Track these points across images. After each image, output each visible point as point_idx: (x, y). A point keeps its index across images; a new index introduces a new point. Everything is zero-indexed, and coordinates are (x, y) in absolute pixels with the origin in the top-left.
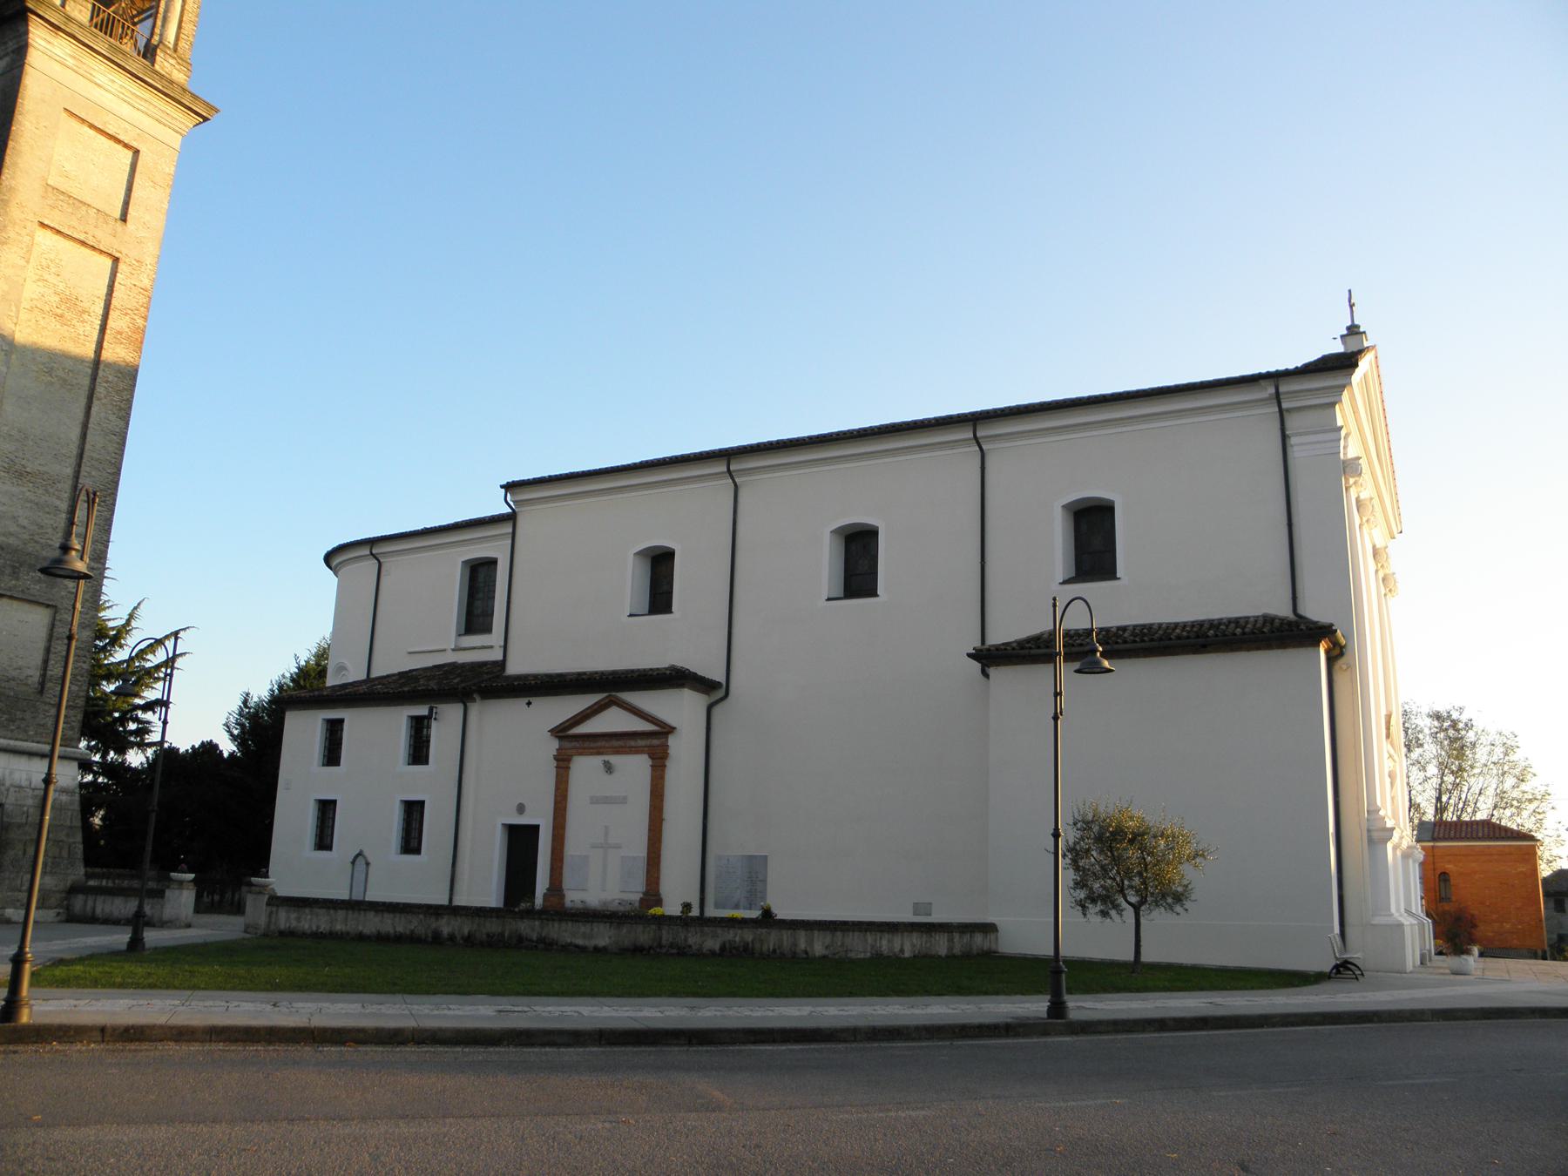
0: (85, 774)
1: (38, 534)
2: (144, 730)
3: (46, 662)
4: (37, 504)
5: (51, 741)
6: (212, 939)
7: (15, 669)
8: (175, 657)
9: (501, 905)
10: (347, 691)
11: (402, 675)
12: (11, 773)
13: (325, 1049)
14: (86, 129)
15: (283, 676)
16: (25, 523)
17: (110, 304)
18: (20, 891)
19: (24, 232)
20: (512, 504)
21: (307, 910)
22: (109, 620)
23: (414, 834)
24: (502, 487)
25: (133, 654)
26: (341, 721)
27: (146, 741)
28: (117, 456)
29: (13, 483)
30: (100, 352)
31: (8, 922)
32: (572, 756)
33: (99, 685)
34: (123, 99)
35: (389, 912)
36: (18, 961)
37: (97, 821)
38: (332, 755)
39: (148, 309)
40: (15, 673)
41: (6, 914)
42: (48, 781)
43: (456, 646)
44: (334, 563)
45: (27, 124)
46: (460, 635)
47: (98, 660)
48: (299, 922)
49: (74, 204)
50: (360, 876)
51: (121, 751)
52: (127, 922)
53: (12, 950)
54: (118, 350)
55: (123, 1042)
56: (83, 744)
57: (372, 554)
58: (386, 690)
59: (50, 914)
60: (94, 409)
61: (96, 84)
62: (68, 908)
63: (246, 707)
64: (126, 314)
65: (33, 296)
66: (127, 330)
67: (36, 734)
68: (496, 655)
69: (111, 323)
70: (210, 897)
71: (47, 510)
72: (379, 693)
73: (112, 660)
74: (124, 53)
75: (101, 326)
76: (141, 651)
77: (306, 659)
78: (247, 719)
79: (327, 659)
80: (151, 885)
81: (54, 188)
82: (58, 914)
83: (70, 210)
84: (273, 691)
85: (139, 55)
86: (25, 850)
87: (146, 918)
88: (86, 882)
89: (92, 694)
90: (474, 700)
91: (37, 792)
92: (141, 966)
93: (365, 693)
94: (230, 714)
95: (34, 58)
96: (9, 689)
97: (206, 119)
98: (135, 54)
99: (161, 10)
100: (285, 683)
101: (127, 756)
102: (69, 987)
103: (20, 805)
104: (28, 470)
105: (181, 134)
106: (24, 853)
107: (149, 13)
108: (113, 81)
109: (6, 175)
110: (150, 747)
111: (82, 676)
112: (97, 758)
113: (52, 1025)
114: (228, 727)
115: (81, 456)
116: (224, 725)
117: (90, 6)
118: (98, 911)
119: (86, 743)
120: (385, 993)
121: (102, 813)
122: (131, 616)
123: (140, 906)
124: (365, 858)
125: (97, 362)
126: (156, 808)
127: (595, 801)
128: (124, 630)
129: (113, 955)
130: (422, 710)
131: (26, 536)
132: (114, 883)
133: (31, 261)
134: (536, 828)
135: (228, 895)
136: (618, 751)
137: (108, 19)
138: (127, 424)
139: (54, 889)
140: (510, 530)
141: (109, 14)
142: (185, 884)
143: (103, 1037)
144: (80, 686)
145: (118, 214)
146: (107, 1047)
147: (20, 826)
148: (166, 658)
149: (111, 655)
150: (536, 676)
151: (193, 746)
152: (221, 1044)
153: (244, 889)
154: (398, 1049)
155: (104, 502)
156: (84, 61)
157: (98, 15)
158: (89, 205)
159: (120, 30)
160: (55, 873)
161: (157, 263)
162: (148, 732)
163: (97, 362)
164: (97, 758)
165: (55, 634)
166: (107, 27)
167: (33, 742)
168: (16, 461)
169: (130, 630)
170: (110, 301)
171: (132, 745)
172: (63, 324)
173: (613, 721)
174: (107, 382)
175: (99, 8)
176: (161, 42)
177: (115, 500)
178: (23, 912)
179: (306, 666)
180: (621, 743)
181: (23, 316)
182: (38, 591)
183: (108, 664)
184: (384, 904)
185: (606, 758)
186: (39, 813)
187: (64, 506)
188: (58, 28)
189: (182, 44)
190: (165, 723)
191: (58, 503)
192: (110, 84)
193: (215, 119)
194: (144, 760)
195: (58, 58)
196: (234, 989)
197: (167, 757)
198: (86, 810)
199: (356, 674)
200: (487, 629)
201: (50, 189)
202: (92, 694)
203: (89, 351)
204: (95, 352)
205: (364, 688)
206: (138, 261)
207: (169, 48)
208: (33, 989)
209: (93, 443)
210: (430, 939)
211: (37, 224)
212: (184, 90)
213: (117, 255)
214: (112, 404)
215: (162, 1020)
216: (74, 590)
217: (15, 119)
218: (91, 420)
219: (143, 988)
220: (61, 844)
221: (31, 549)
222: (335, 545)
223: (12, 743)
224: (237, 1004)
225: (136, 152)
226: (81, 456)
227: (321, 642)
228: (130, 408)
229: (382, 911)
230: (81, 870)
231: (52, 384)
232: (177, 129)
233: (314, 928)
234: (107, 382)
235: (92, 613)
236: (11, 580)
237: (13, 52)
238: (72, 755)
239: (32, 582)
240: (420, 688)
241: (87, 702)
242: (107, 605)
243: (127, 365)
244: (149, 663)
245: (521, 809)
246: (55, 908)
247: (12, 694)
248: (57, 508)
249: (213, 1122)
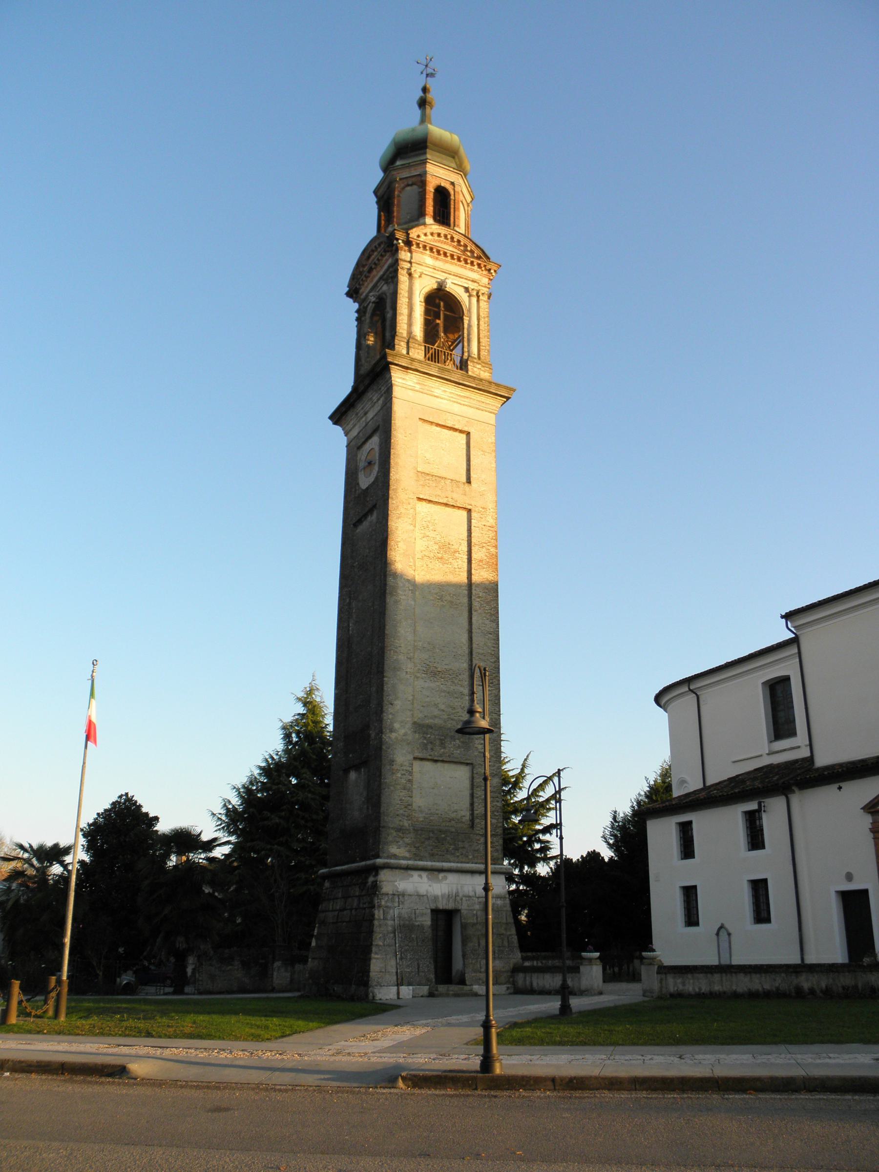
0: (510, 884)
1: (453, 714)
2: (545, 848)
3: (472, 804)
4: (448, 693)
5: (484, 862)
6: (620, 1003)
7: (453, 812)
8: (560, 790)
9: (846, 961)
10: (691, 798)
11: (731, 780)
12: (462, 887)
13: (730, 1096)
14: (434, 428)
15: (639, 794)
16: (442, 707)
17: (471, 542)
18: (481, 972)
19: (409, 507)
20: (793, 629)
21: (690, 976)
22: (509, 771)
23: (763, 907)
24: (782, 617)
25: (530, 793)
26: (690, 823)
27: (548, 856)
28: (495, 649)
29: (431, 681)
30: (471, 578)
31: (476, 995)
33: (510, 818)
34: (452, 401)
35: (756, 973)
36: (486, 1026)
37: (523, 918)
38: (687, 850)
39: (496, 540)
40: (453, 815)
41: (474, 990)
42: (486, 889)
43: (769, 751)
44: (663, 702)
45: (400, 435)
46: (771, 742)
47: (506, 801)
49: (436, 480)
50: (724, 945)
51: (532, 865)
52: (556, 992)
53: (481, 1017)
54: (482, 573)
55: (570, 1090)
56: (506, 862)
57: (690, 690)
58: (721, 794)
59: (503, 988)
60: (474, 619)
61: (435, 396)
62: (514, 983)
63: (616, 821)
64: (483, 547)
65: (422, 549)
66: (486, 558)
67: (474, 857)
68: (805, 753)
69: (474, 556)
70: (612, 970)
71: (456, 695)
72: (716, 797)
73: (516, 799)
74: (448, 371)
75: (468, 559)
76: (535, 790)
77: (654, 779)
78: (618, 831)
79: (670, 777)
80: (569, 963)
81: (422, 473)
82: (508, 988)
83: (434, 485)
84: (634, 807)
85: (457, 369)
86: (479, 942)
87: (569, 989)
88: (523, 963)
89: (506, 825)
90: (793, 792)
91: (481, 900)
92: (572, 1027)
93: (705, 798)
94: (605, 828)
95: (397, 392)
96: (452, 826)
97: (508, 398)
98: (455, 369)
99: (465, 335)
100: (641, 800)
101: (537, 869)
102: (524, 1045)
103: (471, 910)
104: (439, 670)
105: (494, 413)
106: (479, 945)
107: (458, 341)
108: (445, 391)
109: (393, 472)
110: (551, 860)
111: (498, 812)
112: (516, 872)
113: (517, 1076)
114: (605, 838)
115: (471, 653)
116: (602, 837)
117: (423, 348)
118: (535, 984)
119: (507, 862)
120: (769, 1044)
121: (526, 911)
122: (524, 766)
123: (564, 980)
124: (727, 930)
125: (470, 584)
126: (565, 905)
128: (520, 776)
129: (550, 1018)
130: (753, 806)
131: (446, 717)
132: (542, 963)
133: (417, 525)
135: (625, 967)
137: (435, 352)
138: (498, 624)
139: (503, 970)
140: (796, 651)
141: (435, 349)
142: (593, 961)
143: (554, 1086)
144: (497, 819)
145: (464, 479)
146: (559, 1095)
147: (474, 925)
148: (554, 792)
149: (514, 796)
150: (841, 765)
151: (582, 856)
152: (644, 1092)
153: (637, 962)
154: (793, 1097)
155: (492, 683)
156: (425, 384)
157: (429, 352)
158: (445, 478)
159: (443, 357)
160: (502, 958)
161: (496, 506)
162: (549, 849)
163: (470, 584)
164: (516, 872)
165: (475, 784)
166: (435, 358)
167: (472, 863)
168: (431, 664)
169: (524, 776)
170: (471, 540)
171: (539, 860)
172: (444, 564)
174: (479, 597)
175: (429, 347)
176: (469, 356)
177: (499, 681)
178: (484, 988)
179: (655, 785)
181: (419, 563)
182: (459, 754)
183: (513, 803)
184: (750, 966)
186: (484, 914)
187: (466, 691)
188: (407, 368)
189: (482, 353)
190: (561, 838)
191: (462, 689)
192: (443, 393)
193: (514, 397)
194: (549, 870)
195: (410, 387)
196: (645, 1044)
197: (565, 864)
198: (516, 913)
199: (694, 784)
200: (792, 733)
201: (420, 474)
202: (506, 825)
203: (463, 578)
204: (468, 578)
205: (703, 795)
206: (483, 508)
207: (475, 358)
208: (500, 1047)
209: (477, 643)
210: (794, 994)
211: (416, 499)
212: (490, 382)
213: (469, 507)
214: (485, 612)
215: (595, 1072)
216: (483, 750)
217: (392, 435)
218: (474, 626)
219: (577, 1045)
220: (502, 936)
221: (449, 725)
222: (661, 688)
223: (459, 865)
224: (650, 1057)
225: (468, 434)
226: (471, 653)
227: (663, 764)
228: (498, 613)
229: (750, 973)
230: (519, 955)
231: (443, 606)
232: (491, 410)
233: (697, 990)
234: (479, 597)
235: (497, 765)
236: (440, 749)
237: (385, 393)
238: (502, 871)
239: (454, 747)
240: (747, 788)
241: (504, 832)
242: (506, 760)
243: (490, 583)
244: (541, 798)
245: (849, 877)
246: (505, 984)
247: (453, 830)
248: (462, 694)
249: (652, 1165)
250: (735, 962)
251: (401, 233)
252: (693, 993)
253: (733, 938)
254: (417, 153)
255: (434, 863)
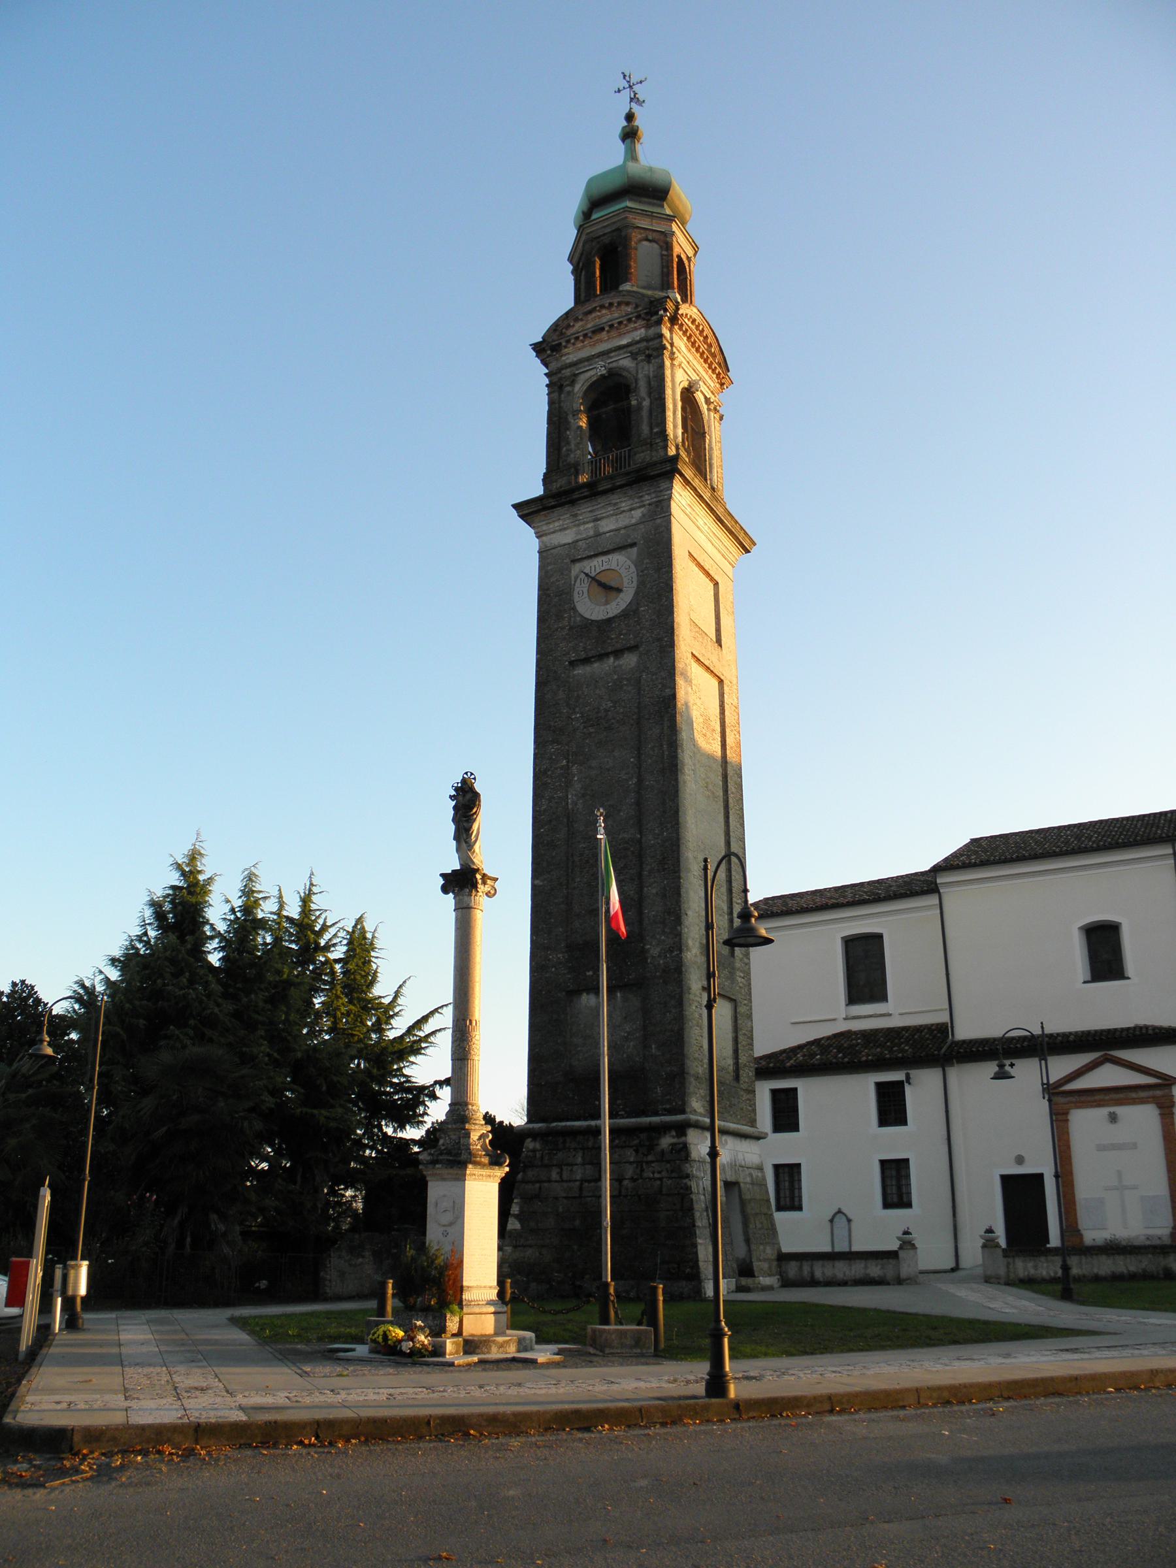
3: (736, 1051)
21: (1043, 1259)
32: (1069, 1109)
35: (1119, 1254)
48: (1036, 1270)
90: (952, 1065)
127: (1102, 1148)
134: (1040, 1177)
136: (1120, 1103)
173: (1108, 1076)
180: (1121, 1096)
185: (1112, 1109)
210: (1162, 1276)
229: (1113, 1254)
233: (1052, 1274)
245: (1020, 1160)
250: (855, 1248)
251: (672, 304)
252: (1048, 1278)
253: (853, 1225)
254: (651, 200)
255: (739, 1127)
